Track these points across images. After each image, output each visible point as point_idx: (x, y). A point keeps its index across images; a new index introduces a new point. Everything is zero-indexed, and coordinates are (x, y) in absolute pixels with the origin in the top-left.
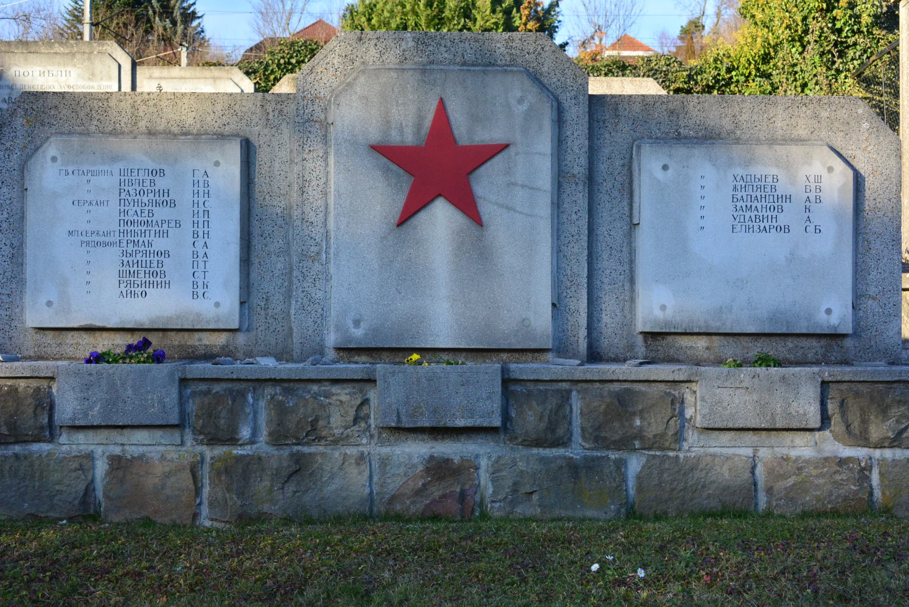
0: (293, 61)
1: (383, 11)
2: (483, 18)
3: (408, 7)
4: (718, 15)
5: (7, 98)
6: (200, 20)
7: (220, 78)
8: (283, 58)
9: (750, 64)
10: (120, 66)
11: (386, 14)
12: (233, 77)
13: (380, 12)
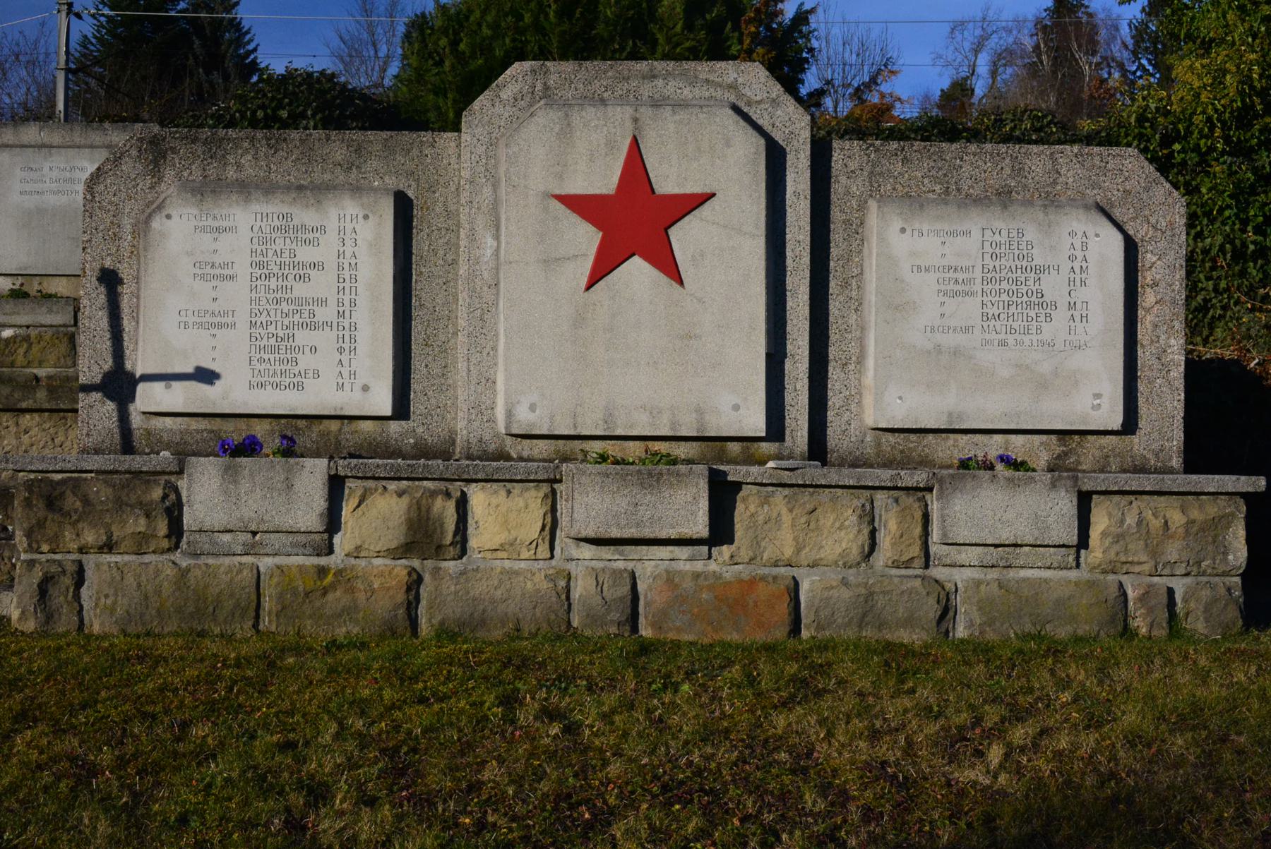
1: (480, 25)
2: (669, 40)
3: (528, 18)
4: (994, 74)
8: (263, 107)
9: (1212, 128)
11: (486, 31)
13: (474, 28)
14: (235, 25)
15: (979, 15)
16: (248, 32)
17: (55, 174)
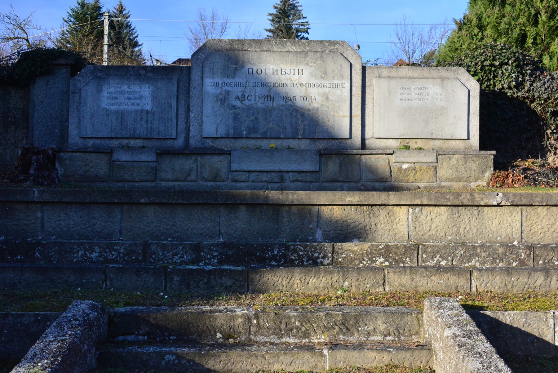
0: (497, 63)
5: (240, 95)
6: (140, 47)
7: (448, 78)
10: (351, 65)
12: (459, 77)
14: (128, 26)
15: (443, 22)
16: (134, 29)
17: (416, 91)
